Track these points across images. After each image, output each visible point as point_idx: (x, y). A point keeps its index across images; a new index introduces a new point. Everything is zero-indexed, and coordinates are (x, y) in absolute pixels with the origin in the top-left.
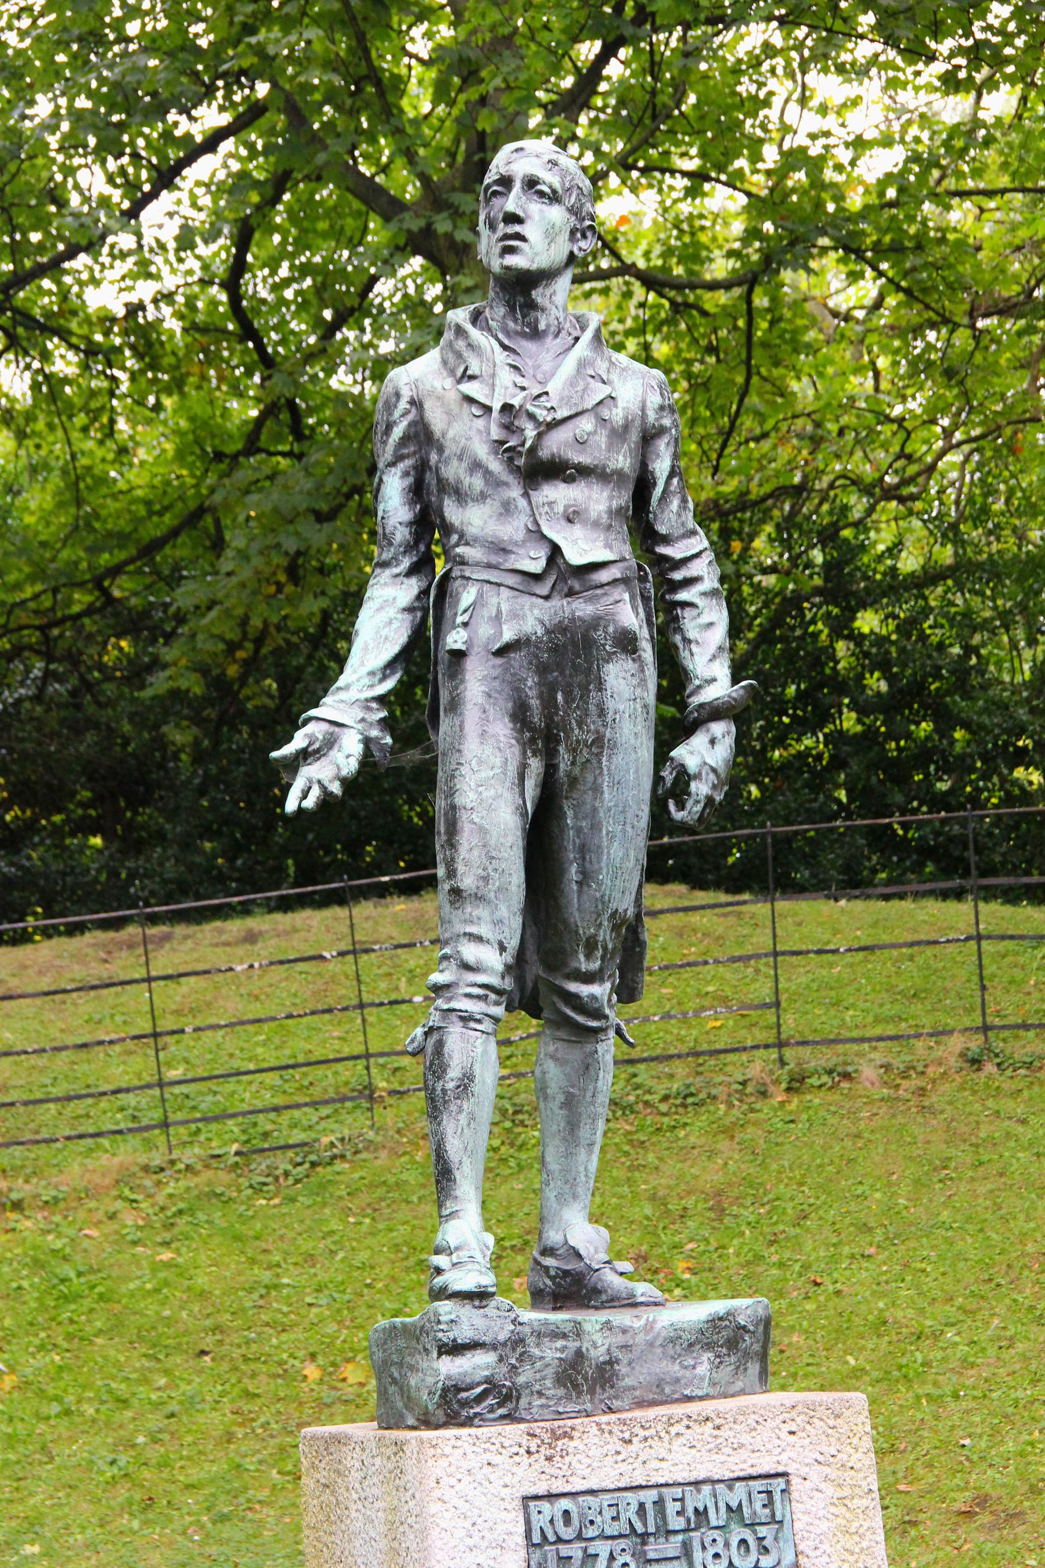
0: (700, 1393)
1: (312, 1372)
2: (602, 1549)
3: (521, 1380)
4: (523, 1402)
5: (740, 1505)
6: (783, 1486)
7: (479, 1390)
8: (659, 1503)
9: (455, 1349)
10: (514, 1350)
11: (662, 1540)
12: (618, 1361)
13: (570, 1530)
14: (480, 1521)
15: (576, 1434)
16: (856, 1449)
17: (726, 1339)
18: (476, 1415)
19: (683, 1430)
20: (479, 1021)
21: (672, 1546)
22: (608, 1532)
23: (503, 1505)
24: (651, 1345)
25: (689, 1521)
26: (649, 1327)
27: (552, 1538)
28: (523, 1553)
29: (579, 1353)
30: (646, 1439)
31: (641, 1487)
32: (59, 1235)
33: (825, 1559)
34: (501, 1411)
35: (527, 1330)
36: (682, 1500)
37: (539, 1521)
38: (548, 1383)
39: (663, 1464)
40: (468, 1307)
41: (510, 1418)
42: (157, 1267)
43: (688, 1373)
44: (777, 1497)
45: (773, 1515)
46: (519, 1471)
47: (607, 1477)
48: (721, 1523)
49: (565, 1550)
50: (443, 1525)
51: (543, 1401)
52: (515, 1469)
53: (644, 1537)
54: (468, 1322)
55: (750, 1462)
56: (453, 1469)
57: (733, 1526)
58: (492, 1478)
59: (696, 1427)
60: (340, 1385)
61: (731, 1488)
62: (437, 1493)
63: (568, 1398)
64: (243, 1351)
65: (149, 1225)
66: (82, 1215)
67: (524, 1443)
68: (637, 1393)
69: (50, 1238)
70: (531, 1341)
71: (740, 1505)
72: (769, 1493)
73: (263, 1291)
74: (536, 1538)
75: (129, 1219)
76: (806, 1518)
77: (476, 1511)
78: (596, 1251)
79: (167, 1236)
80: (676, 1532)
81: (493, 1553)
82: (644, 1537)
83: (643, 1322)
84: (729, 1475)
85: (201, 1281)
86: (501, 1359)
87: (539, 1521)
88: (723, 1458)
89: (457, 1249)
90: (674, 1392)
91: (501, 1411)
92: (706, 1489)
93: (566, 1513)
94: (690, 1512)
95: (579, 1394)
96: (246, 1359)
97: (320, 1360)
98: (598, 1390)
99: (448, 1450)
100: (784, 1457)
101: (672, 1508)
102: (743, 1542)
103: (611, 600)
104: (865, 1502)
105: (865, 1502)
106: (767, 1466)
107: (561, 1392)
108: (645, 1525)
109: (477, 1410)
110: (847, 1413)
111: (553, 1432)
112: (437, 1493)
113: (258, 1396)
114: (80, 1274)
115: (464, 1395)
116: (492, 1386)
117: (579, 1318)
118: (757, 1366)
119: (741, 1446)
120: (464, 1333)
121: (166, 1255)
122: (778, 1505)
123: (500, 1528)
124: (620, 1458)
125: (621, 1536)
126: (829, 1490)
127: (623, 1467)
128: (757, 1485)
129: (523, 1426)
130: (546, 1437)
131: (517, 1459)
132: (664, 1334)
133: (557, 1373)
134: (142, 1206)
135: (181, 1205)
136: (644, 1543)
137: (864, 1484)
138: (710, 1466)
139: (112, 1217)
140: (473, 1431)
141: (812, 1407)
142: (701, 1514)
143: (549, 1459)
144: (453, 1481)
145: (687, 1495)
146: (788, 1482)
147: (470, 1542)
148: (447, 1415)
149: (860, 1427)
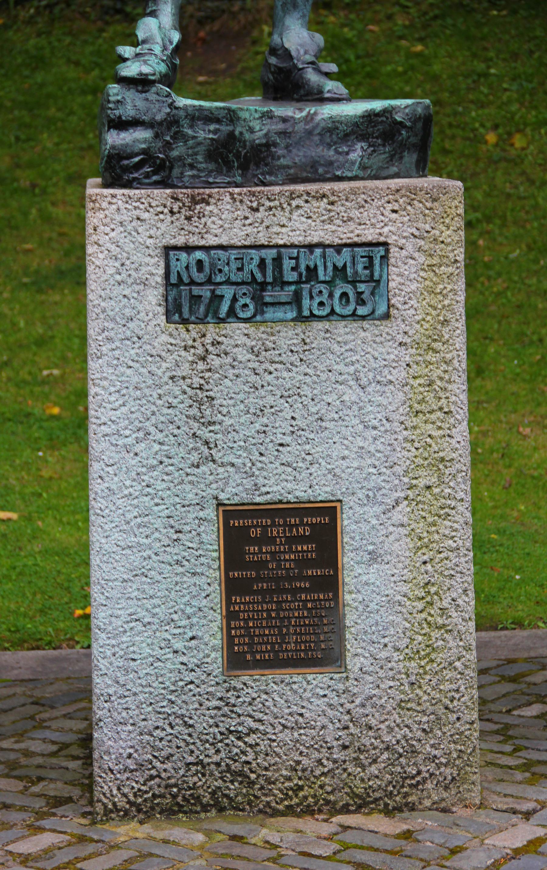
0: (350, 175)
1: (492, 138)
2: (228, 292)
3: (175, 153)
4: (176, 172)
5: (345, 265)
6: (383, 253)
7: (137, 159)
9: (121, 125)
10: (169, 129)
11: (278, 288)
12: (275, 145)
13: (202, 275)
14: (128, 262)
15: (212, 201)
16: (448, 228)
17: (377, 130)
18: (135, 179)
19: (302, 204)
22: (233, 278)
23: (148, 252)
24: (310, 133)
25: (300, 275)
26: (310, 118)
27: (186, 279)
28: (161, 290)
29: (231, 135)
30: (270, 209)
31: (263, 246)
32: (352, 29)
33: (412, 311)
34: (155, 178)
35: (182, 113)
36: (297, 258)
37: (177, 267)
38: (200, 158)
39: (284, 230)
40: (132, 91)
41: (164, 184)
42: (410, 55)
43: (341, 158)
44: (377, 262)
45: (372, 275)
46: (163, 227)
47: (237, 235)
48: (328, 279)
49: (196, 290)
50: (98, 263)
51: (195, 172)
52: (159, 225)
53: (263, 286)
54: (131, 104)
55: (357, 232)
56: (108, 220)
57: (338, 282)
58: (140, 230)
59: (315, 203)
60: (508, 148)
61: (339, 252)
62: (94, 238)
63: (219, 172)
64: (451, 119)
65: (412, 26)
66: (369, 15)
67: (169, 204)
68: (292, 171)
69: (346, 30)
70: (185, 123)
71: (345, 265)
72: (371, 258)
73: (475, 78)
74: (174, 279)
75: (400, 21)
76: (399, 279)
77: (125, 255)
78: (306, 52)
79: (423, 34)
80: (290, 283)
81: (137, 288)
82: (263, 286)
83: (304, 114)
84: (337, 241)
85: (436, 68)
86: (157, 136)
87: (177, 267)
88: (334, 228)
89: (144, 42)
90: (326, 172)
91: (155, 178)
92: (318, 251)
94: (303, 267)
95: (230, 168)
96: (450, 125)
97: (501, 130)
98: (252, 166)
99: (104, 205)
100: (386, 230)
101: (288, 264)
102: (344, 295)
104: (450, 270)
105: (450, 270)
106: (370, 235)
107: (212, 166)
108: (264, 276)
109: (136, 175)
110: (443, 198)
111: (193, 197)
112: (94, 238)
113: (451, 152)
114: (358, 57)
115: (126, 162)
116: (148, 156)
117: (234, 106)
118: (415, 156)
119: (350, 219)
120: (128, 111)
121: (419, 48)
122: (377, 267)
123: (144, 269)
124: (247, 222)
125: (243, 283)
126: (421, 258)
127: (249, 230)
128: (360, 251)
129: (168, 191)
130: (187, 201)
131: (161, 216)
132: (323, 124)
133: (209, 151)
134: (411, 11)
135: (437, 12)
136: (263, 290)
137: (451, 255)
138: (322, 233)
139: (390, 17)
140: (126, 191)
141: (413, 191)
142: (312, 272)
143: (188, 218)
144: (107, 230)
145: (302, 255)
146: (387, 251)
147: (118, 278)
148: (113, 178)
149: (453, 211)
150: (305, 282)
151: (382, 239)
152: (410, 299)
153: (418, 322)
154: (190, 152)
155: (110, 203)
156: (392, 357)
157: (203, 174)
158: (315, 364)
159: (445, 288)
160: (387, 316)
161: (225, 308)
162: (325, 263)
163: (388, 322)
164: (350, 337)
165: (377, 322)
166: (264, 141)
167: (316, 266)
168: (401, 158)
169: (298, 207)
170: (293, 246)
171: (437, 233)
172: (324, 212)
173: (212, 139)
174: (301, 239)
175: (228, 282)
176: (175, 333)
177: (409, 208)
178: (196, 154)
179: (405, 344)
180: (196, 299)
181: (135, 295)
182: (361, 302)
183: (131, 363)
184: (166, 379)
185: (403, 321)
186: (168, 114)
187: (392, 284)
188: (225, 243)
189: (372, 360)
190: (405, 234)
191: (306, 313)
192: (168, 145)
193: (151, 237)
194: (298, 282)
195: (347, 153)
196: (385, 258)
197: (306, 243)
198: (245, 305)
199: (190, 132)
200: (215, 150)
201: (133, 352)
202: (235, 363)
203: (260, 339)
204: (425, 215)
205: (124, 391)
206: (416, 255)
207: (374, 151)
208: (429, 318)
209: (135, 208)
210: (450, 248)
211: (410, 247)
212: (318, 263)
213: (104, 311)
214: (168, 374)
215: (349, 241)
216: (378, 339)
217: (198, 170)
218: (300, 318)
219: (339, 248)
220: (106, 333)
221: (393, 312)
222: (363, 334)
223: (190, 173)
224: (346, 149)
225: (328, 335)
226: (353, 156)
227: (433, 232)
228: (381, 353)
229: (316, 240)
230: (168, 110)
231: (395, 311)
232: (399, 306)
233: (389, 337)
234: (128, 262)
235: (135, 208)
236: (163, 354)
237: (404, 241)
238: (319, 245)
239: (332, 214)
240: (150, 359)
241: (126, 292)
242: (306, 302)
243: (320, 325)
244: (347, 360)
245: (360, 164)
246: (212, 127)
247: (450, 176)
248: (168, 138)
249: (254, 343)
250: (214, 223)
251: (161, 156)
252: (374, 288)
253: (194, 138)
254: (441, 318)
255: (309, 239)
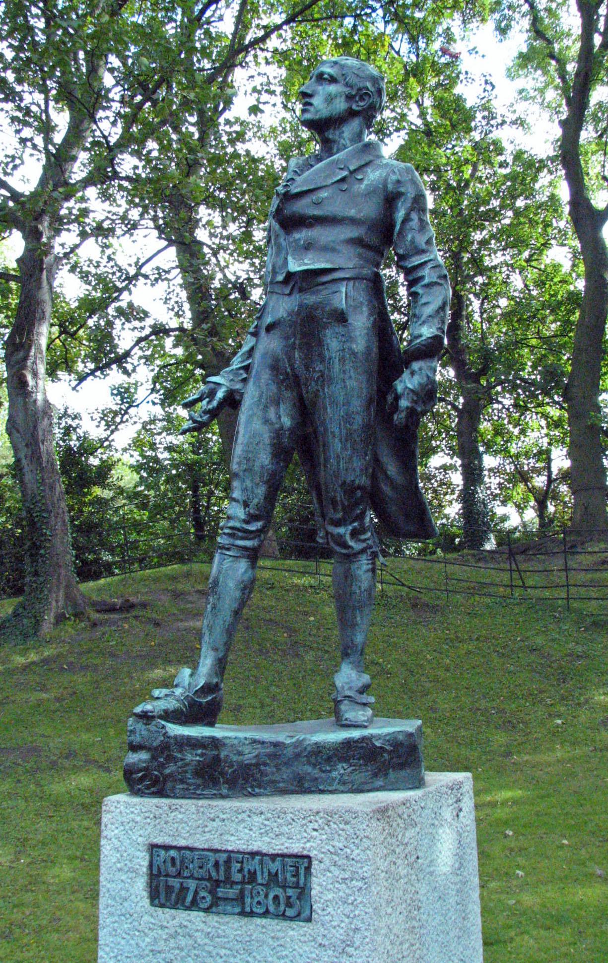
0: (330, 788)
2: (192, 884)
3: (167, 771)
4: (169, 785)
6: (306, 865)
7: (140, 775)
8: (228, 862)
11: (228, 886)
12: (265, 764)
14: (125, 855)
20: (228, 549)
21: (232, 892)
22: (196, 875)
30: (224, 820)
37: (158, 861)
38: (189, 776)
43: (323, 775)
44: (302, 872)
45: (298, 883)
52: (147, 827)
53: (217, 883)
55: (286, 845)
61: (273, 860)
63: (206, 787)
68: (281, 785)
74: (155, 872)
76: (318, 888)
80: (237, 883)
81: (131, 875)
82: (217, 883)
84: (272, 851)
86: (154, 758)
93: (173, 859)
100: (308, 845)
101: (236, 866)
103: (330, 291)
110: (353, 822)
120: (137, 739)
124: (206, 829)
132: (309, 749)
136: (218, 886)
137: (360, 871)
138: (260, 843)
142: (253, 875)
145: (245, 860)
146: (310, 863)
150: (249, 883)
151: (305, 853)
152: (327, 906)
153: (335, 927)
154: (180, 770)
155: (116, 807)
156: (314, 955)
157: (192, 788)
158: (255, 954)
159: (355, 900)
160: (309, 920)
161: (189, 898)
162: (262, 869)
163: (310, 924)
164: (280, 934)
165: (301, 924)
166: (254, 762)
167: (255, 870)
168: (386, 775)
169: (243, 821)
170: (239, 852)
171: (349, 851)
172: (262, 827)
173: (199, 761)
174: (244, 847)
175: (192, 877)
176: (155, 914)
177: (326, 827)
178: (186, 772)
179: (324, 946)
180: (169, 889)
181: (129, 881)
182: (289, 905)
183: (124, 935)
184: (147, 952)
185: (323, 925)
186: (162, 741)
187: (313, 892)
188: (190, 846)
189: (298, 957)
190: (323, 850)
191: (248, 909)
192: (162, 766)
193: (141, 836)
194: (242, 883)
195: (330, 771)
196: (308, 869)
197: (248, 850)
198: (204, 898)
199: (179, 756)
200: (202, 769)
201: (126, 926)
202: (196, 945)
203: (214, 927)
204: (339, 835)
205: (119, 958)
206: (332, 868)
207: (356, 770)
208: (343, 925)
209: (132, 812)
210: (359, 865)
211: (327, 862)
212: (257, 869)
213: (108, 891)
214: (149, 948)
215: (280, 852)
216: (302, 939)
217: (187, 784)
218: (243, 914)
219: (274, 857)
220: (109, 909)
221: (314, 916)
222: (292, 933)
223: (181, 786)
224: (328, 768)
225: (264, 930)
226: (334, 774)
227: (346, 850)
228: (305, 951)
229: (255, 849)
230: (162, 738)
231: (316, 916)
232: (319, 911)
233: (311, 938)
234: (125, 855)
235: (132, 812)
236: (146, 931)
237: (323, 856)
238: (258, 853)
239: (268, 828)
240: (137, 933)
241: (123, 878)
242: (248, 900)
243: (258, 921)
244: (279, 954)
245: (340, 780)
246: (199, 751)
247: (88, 856)
248: (162, 760)
249: (209, 930)
250: (183, 828)
251: (156, 773)
252: (300, 893)
253: (182, 760)
254: (353, 926)
255: (250, 847)
